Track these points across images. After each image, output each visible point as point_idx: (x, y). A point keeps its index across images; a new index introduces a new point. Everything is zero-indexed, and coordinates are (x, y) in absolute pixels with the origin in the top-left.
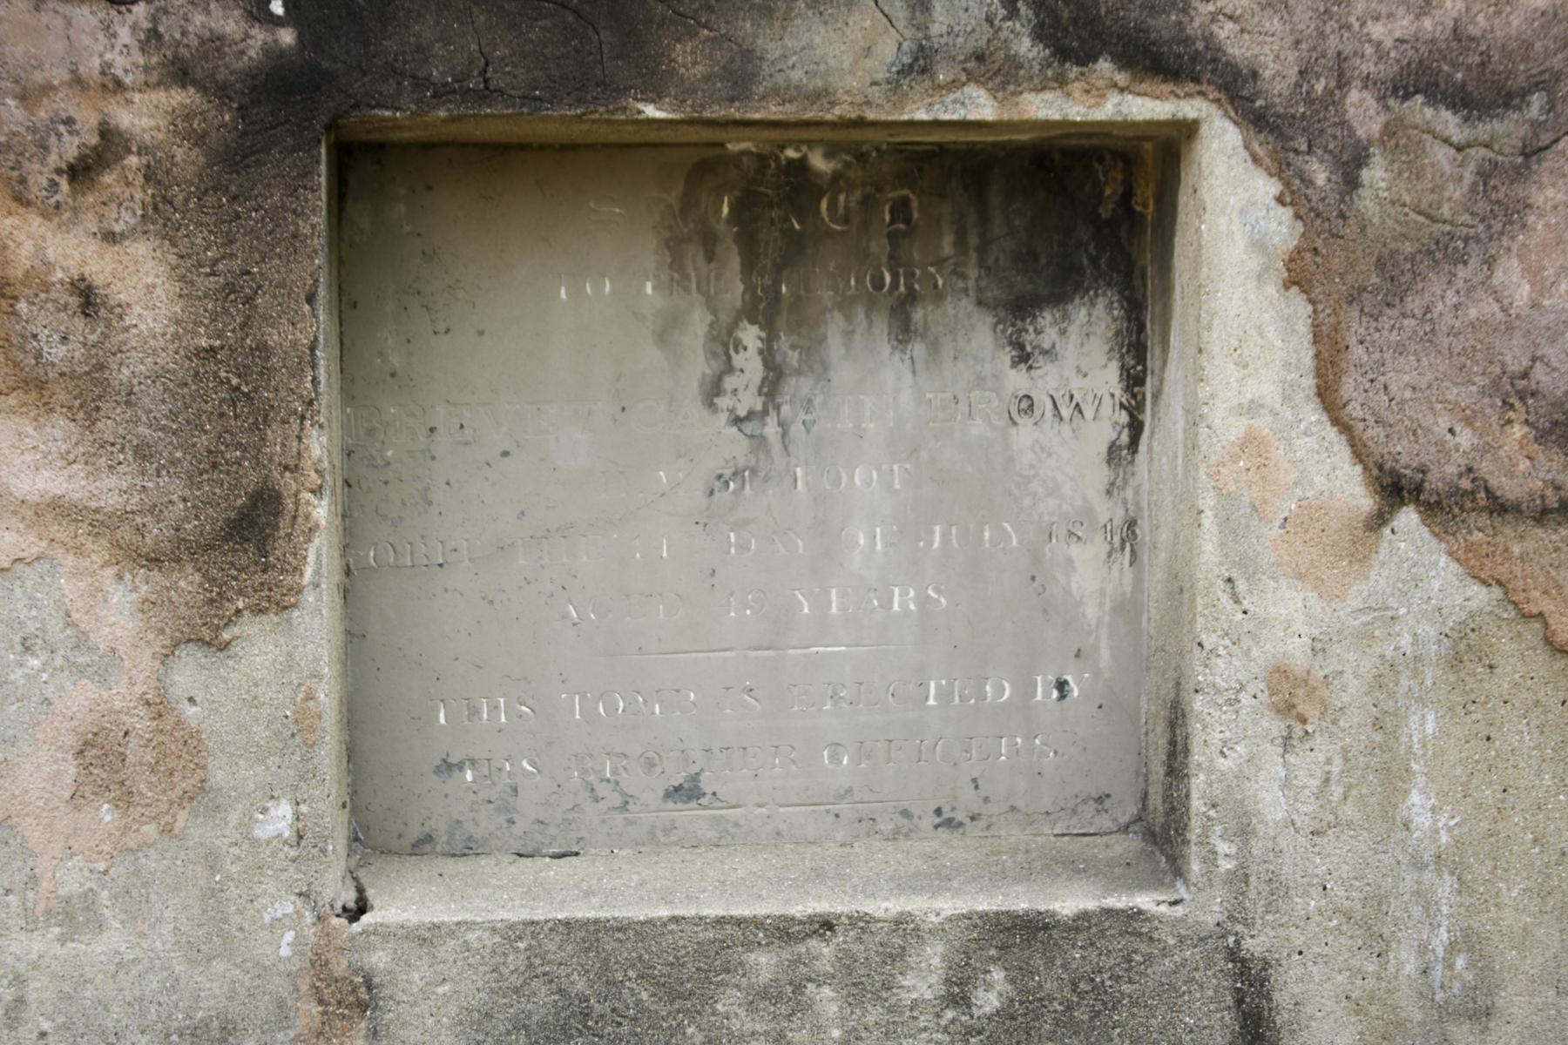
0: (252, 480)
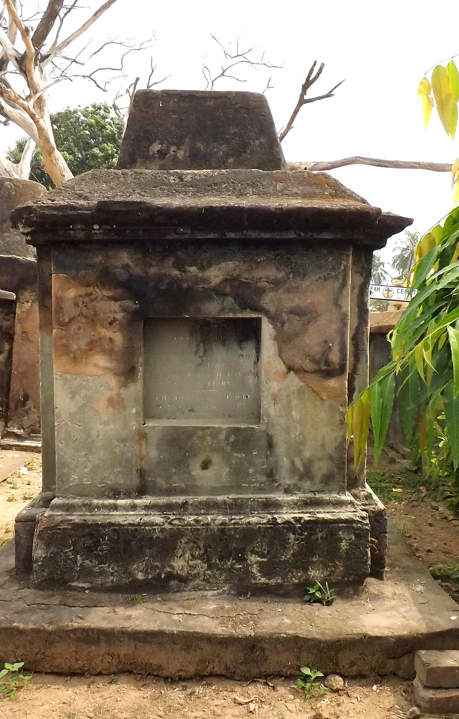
0: (132, 365)
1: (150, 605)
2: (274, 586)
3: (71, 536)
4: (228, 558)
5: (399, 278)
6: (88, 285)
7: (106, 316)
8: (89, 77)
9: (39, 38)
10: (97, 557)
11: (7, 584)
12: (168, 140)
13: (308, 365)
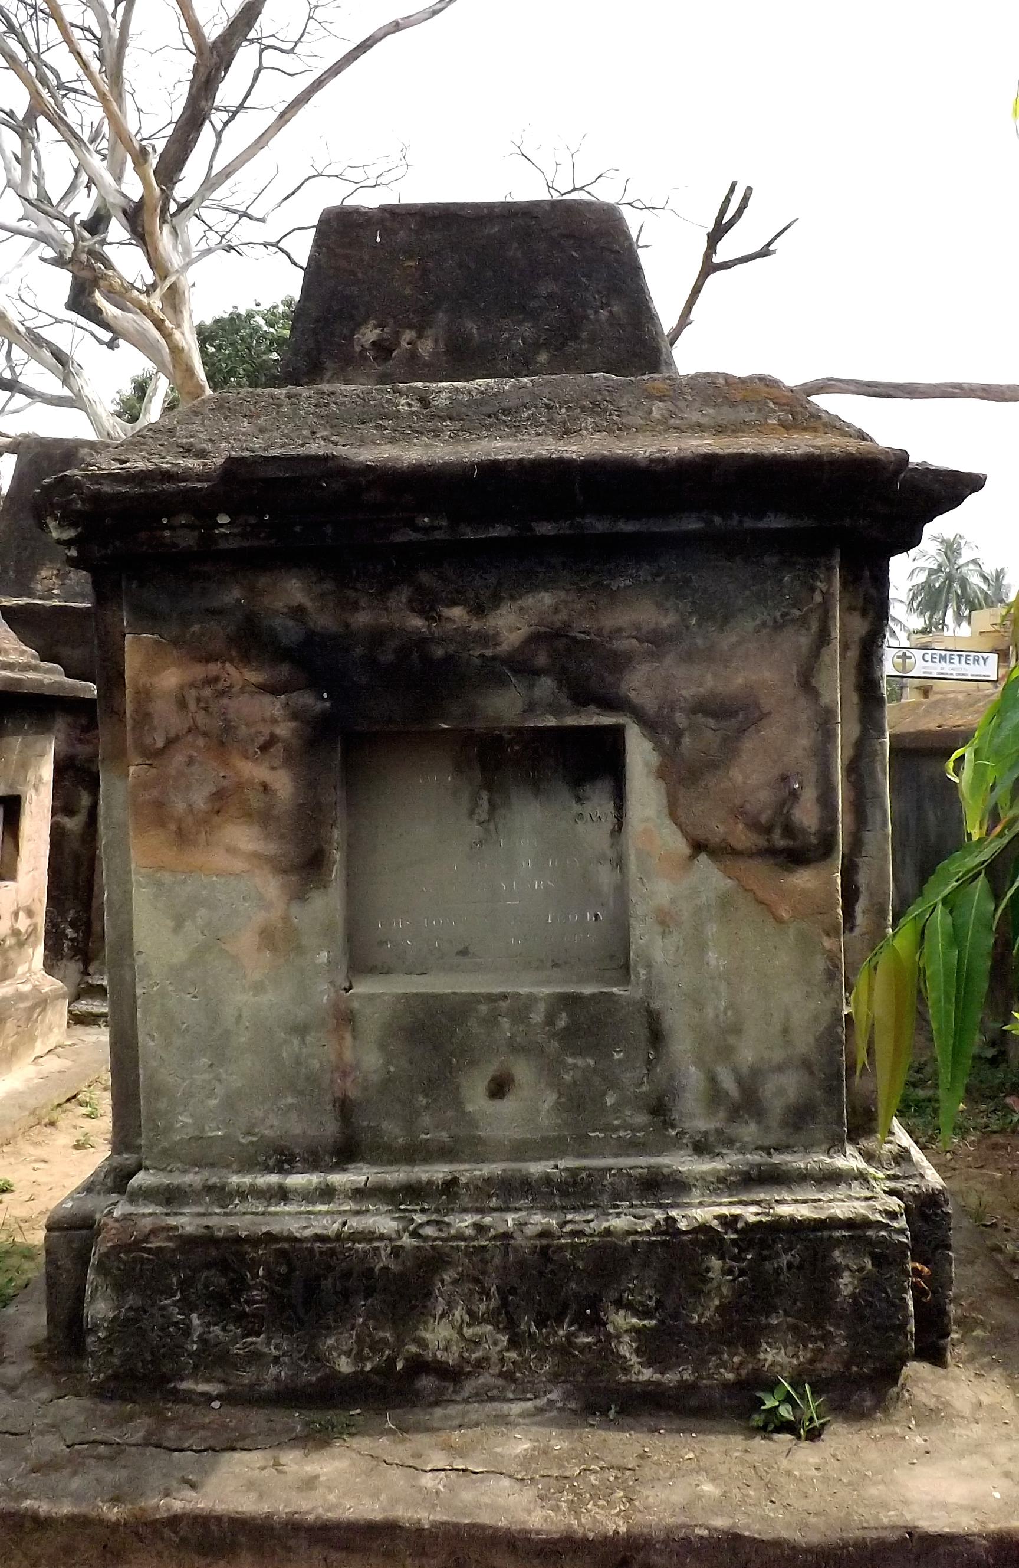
1: (363, 1443)
2: (674, 1387)
3: (175, 1267)
4: (560, 1322)
5: (924, 632)
6: (209, 659)
7: (253, 730)
8: (276, 245)
9: (170, 168)
10: (240, 1317)
11: (25, 1384)
12: (394, 317)
13: (742, 837)
